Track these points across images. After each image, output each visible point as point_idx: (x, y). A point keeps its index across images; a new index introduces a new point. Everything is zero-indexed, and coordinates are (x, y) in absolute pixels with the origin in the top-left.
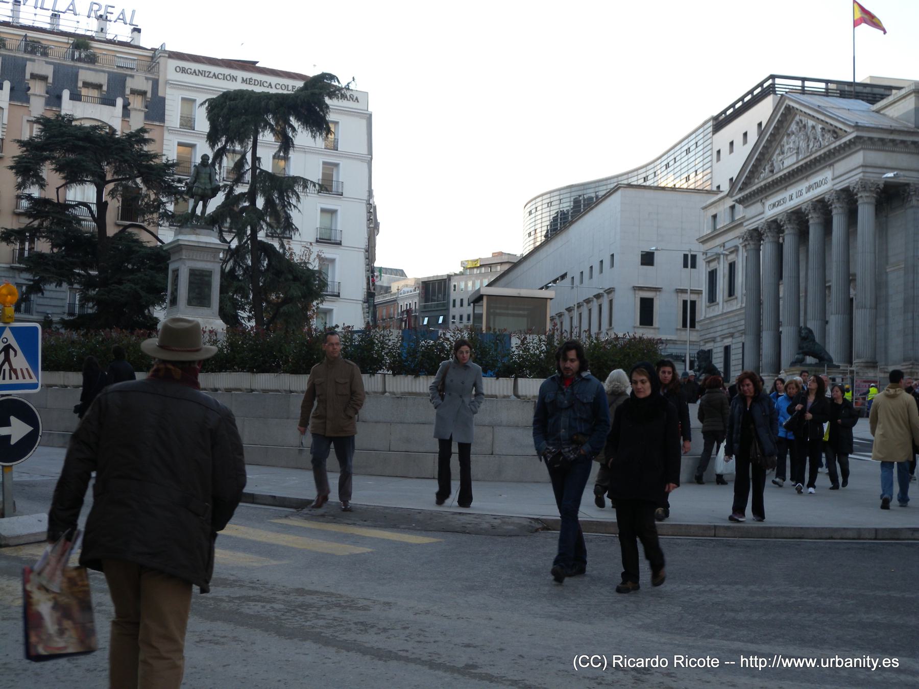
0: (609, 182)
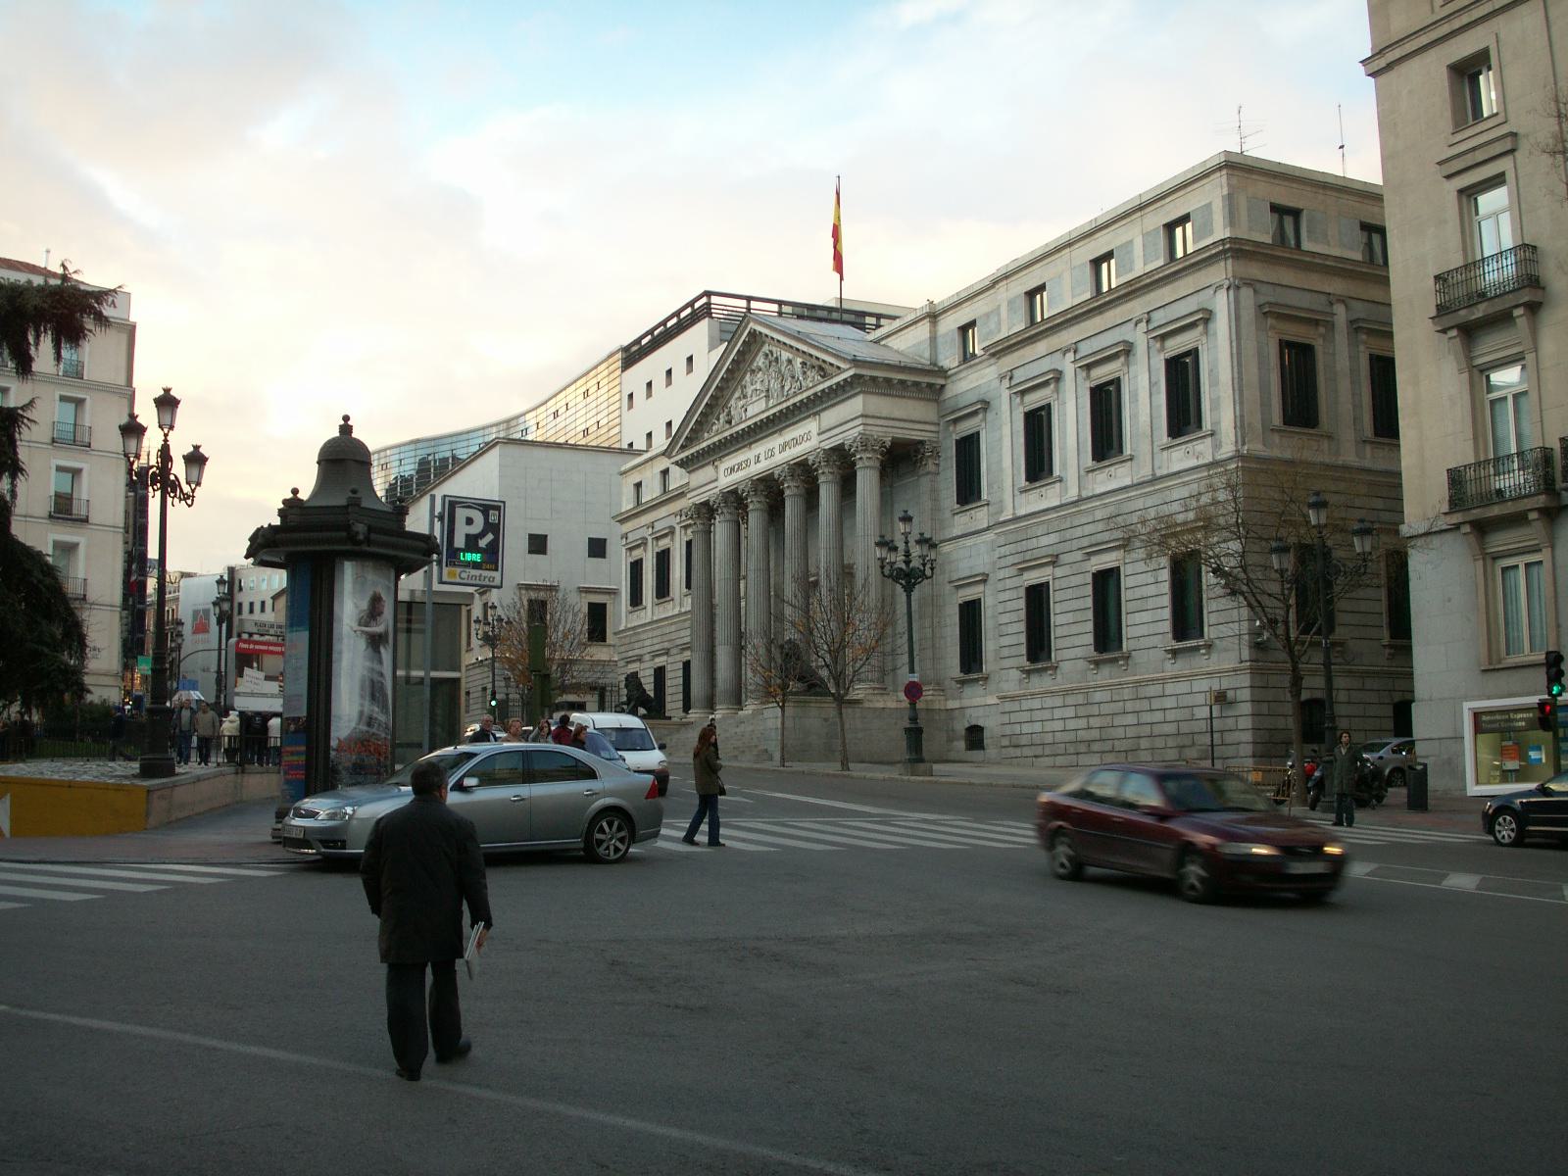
0: (471, 435)
